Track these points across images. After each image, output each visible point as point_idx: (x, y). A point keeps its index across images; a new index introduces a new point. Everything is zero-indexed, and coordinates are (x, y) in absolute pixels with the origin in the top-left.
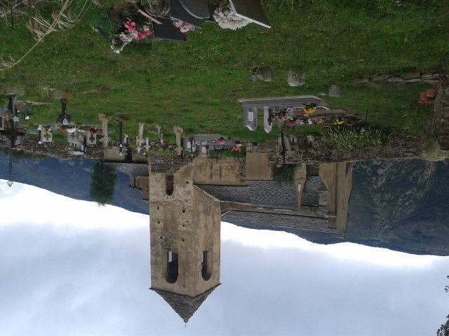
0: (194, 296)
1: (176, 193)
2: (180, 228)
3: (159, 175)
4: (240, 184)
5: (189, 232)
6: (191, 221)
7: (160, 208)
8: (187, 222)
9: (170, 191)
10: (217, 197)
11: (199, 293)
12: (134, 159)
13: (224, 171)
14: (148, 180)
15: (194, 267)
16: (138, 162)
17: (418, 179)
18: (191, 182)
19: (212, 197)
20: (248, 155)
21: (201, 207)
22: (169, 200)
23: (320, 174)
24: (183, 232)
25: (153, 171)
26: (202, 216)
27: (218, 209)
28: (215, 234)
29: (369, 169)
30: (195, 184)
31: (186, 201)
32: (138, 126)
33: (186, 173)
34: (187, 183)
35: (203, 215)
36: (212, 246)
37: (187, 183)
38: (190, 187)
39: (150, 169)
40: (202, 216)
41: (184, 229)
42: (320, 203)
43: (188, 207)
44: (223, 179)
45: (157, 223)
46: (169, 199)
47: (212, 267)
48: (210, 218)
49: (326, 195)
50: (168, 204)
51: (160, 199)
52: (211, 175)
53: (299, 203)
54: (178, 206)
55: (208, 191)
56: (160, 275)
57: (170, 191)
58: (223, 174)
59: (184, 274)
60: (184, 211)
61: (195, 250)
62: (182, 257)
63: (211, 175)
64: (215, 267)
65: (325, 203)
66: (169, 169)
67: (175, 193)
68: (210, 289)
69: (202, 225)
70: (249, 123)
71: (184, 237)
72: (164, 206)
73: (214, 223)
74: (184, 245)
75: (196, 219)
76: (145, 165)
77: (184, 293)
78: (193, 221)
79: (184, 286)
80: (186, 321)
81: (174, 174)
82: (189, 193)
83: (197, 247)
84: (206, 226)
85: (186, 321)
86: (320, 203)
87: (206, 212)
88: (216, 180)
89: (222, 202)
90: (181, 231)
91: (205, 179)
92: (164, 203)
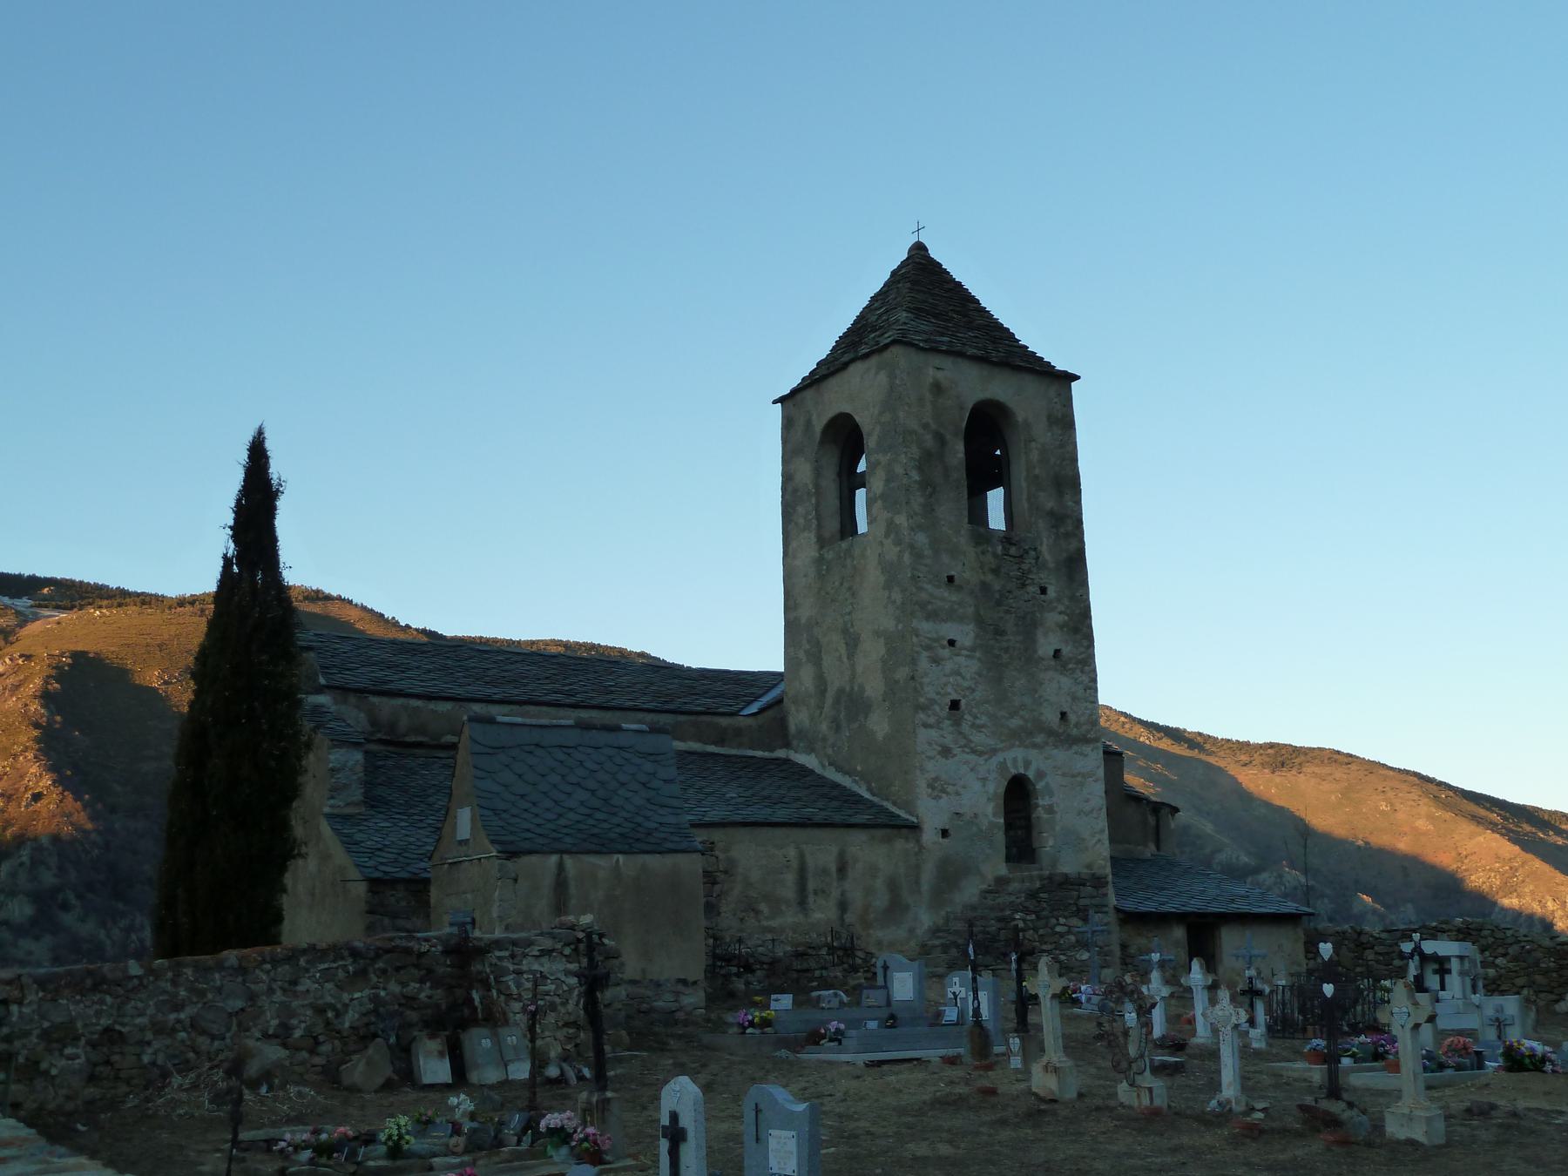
0: (896, 350)
1: (991, 787)
2: (965, 634)
3: (1069, 865)
4: (717, 835)
5: (933, 616)
6: (924, 663)
7: (1056, 718)
8: (936, 661)
9: (1018, 793)
10: (804, 771)
11: (874, 360)
12: (1179, 933)
13: (789, 892)
14: (1112, 840)
15: (899, 470)
16: (1160, 920)
17: (872, 332)
18: (929, 836)
19: (832, 775)
20: (696, 971)
21: (879, 724)
22: (1018, 753)
23: (361, 889)
24: (951, 615)
25: (1098, 882)
26: (874, 687)
27: (798, 718)
28: (806, 612)
29: (68, 919)
30: (915, 828)
31: (946, 752)
32: (1245, 1089)
33: (951, 874)
34: (945, 833)
35: (869, 692)
36: (820, 561)
37: (945, 833)
38: (931, 814)
39: (1110, 891)
40: (874, 687)
41: (950, 630)
42: (358, 756)
43: (937, 725)
44: (792, 853)
45: (1067, 650)
46: (1017, 759)
47: (818, 472)
48: (836, 681)
49: (335, 791)
50: (1019, 737)
51: (1060, 755)
52: (842, 870)
53: (462, 755)
54: (979, 728)
55: (854, 800)
56: (1043, 435)
57: (1018, 793)
58: (790, 878)
59: (941, 439)
60: (955, 705)
61: (898, 542)
62: (951, 508)
63: (842, 870)
64: (805, 472)
65: (336, 757)
66: (1032, 895)
67: (997, 786)
68: (825, 377)
69: (872, 652)
70: (787, 1121)
71: (949, 596)
72: (1039, 726)
73: (816, 657)
74: (945, 558)
75: (902, 674)
76: (1130, 905)
77: (938, 360)
78: (914, 662)
79: (937, 388)
80: (919, 249)
81: (1003, 869)
82: (938, 788)
83: (892, 551)
84: (853, 642)
85: (919, 249)
86: (358, 756)
87: (853, 704)
88: (822, 850)
89: (781, 753)
90: (961, 619)
91: (867, 851)
92: (1039, 739)
